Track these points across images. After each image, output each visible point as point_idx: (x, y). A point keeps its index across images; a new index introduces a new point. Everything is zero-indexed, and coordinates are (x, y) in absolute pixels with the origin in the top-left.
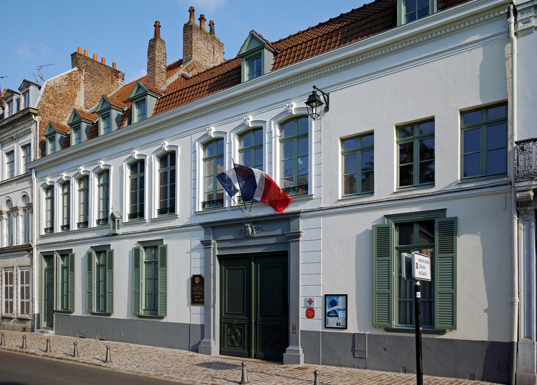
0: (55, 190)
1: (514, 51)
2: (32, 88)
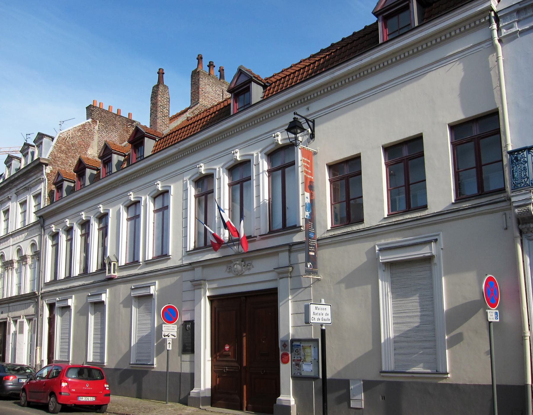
0: (60, 237)
1: (500, 58)
2: (45, 140)
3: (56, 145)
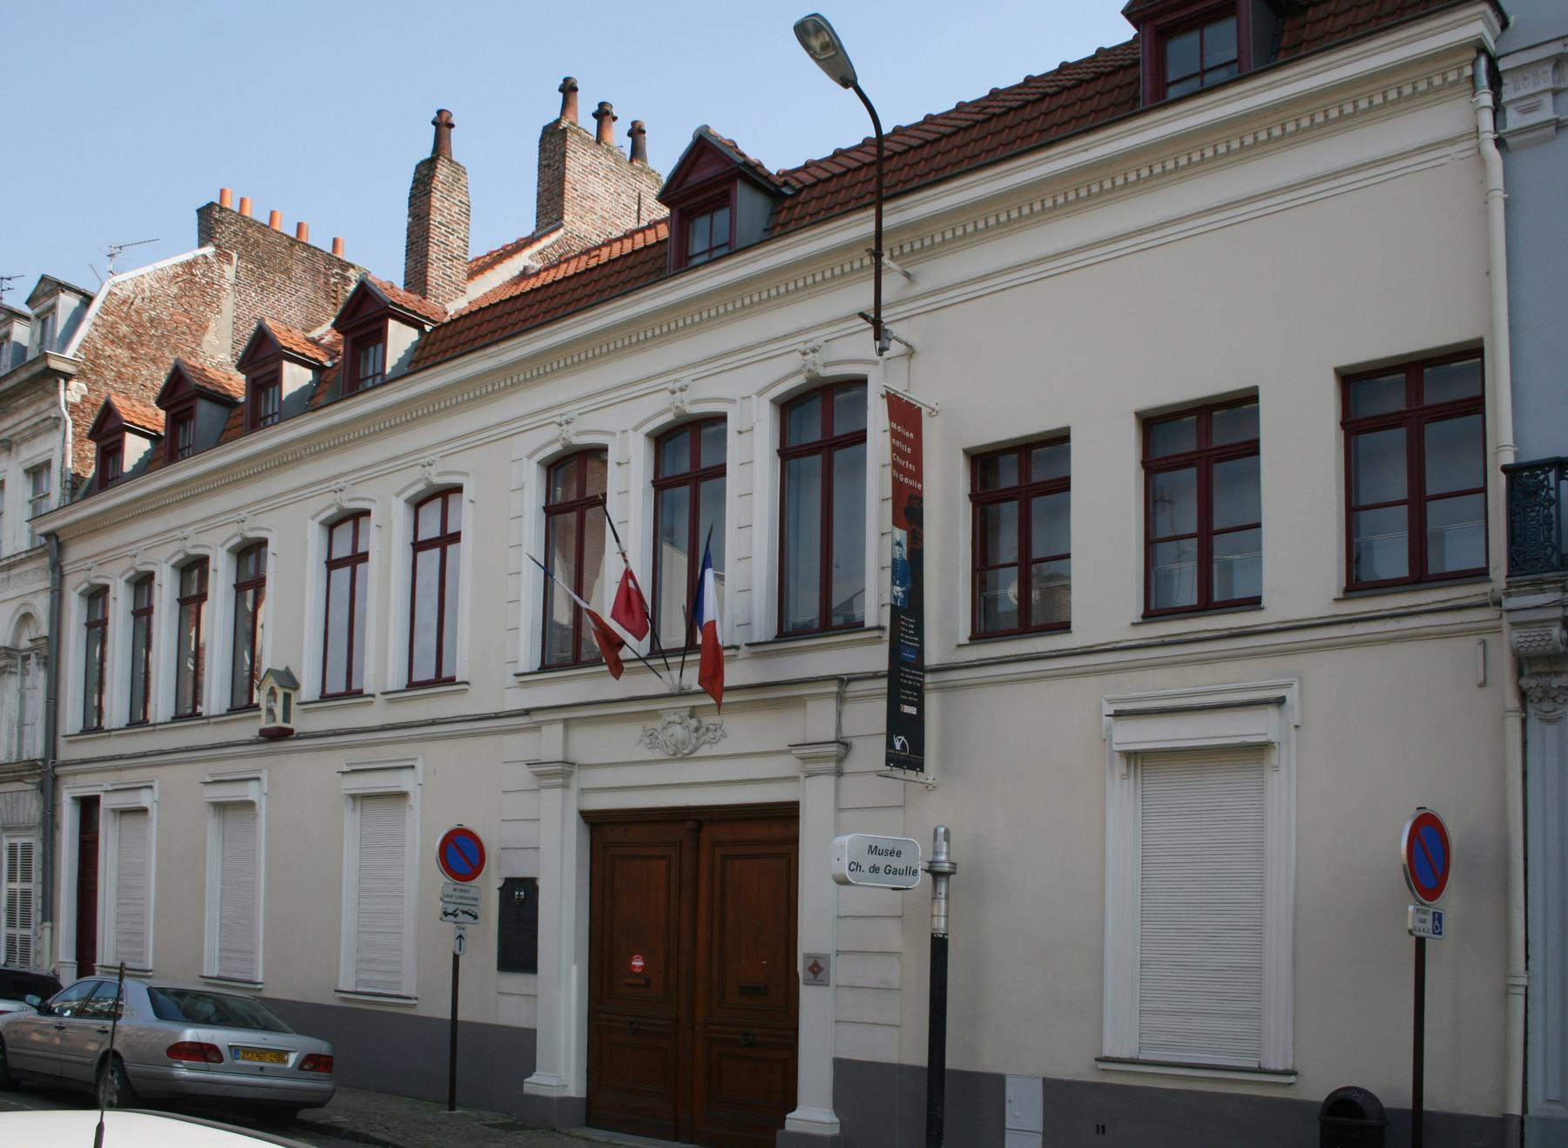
3: (100, 317)
